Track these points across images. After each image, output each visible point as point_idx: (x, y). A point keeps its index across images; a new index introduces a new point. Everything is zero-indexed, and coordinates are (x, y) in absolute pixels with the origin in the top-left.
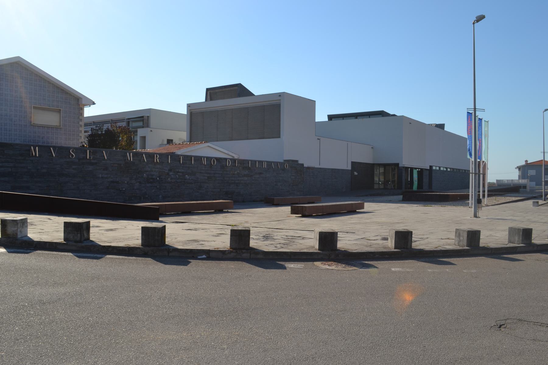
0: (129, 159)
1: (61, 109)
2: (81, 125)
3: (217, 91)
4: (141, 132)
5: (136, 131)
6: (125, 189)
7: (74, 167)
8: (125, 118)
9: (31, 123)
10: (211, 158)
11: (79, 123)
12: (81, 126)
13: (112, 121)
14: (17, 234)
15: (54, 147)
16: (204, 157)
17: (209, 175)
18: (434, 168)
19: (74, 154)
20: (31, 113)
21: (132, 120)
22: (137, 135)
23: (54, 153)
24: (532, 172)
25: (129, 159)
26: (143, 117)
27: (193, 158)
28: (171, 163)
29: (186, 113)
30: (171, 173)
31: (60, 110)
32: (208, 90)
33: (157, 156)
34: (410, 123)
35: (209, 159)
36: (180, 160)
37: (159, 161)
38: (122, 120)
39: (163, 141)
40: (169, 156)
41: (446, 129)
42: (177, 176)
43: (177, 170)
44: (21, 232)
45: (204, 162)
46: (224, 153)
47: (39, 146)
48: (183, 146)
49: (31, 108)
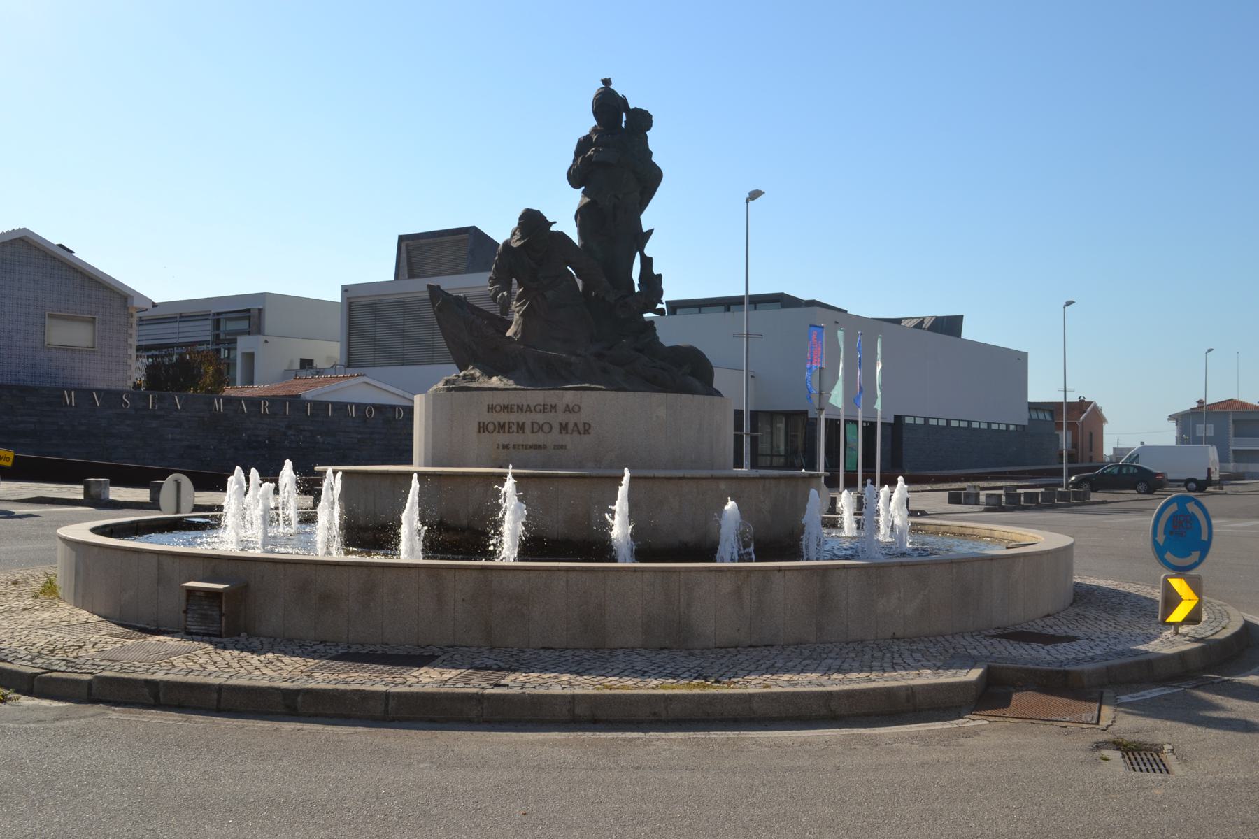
0: (218, 409)
1: (97, 317)
2: (131, 345)
3: (422, 241)
4: (244, 344)
5: (235, 341)
6: (211, 459)
7: (128, 422)
8: (210, 311)
9: (44, 343)
10: (365, 405)
11: (127, 341)
12: (131, 346)
13: (181, 317)
14: (100, 495)
15: (98, 391)
16: (351, 404)
17: (359, 436)
18: (908, 420)
20: (44, 326)
21: (224, 316)
22: (235, 349)
23: (99, 400)
24: (1204, 429)
25: (218, 409)
26: (248, 310)
27: (330, 406)
28: (289, 415)
29: (340, 301)
30: (290, 433)
31: (94, 318)
32: (402, 239)
34: (836, 322)
35: (360, 407)
36: (307, 410)
37: (269, 411)
38: (203, 317)
39: (292, 362)
40: (288, 403)
41: (969, 332)
42: (302, 437)
43: (301, 427)
44: (104, 493)
45: (352, 413)
46: (398, 395)
47: (75, 390)
48: (319, 382)
49: (45, 318)
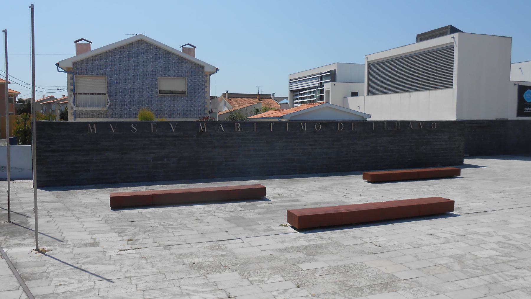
11: (204, 90)
19: (136, 128)
32: (417, 35)
33: (238, 125)
